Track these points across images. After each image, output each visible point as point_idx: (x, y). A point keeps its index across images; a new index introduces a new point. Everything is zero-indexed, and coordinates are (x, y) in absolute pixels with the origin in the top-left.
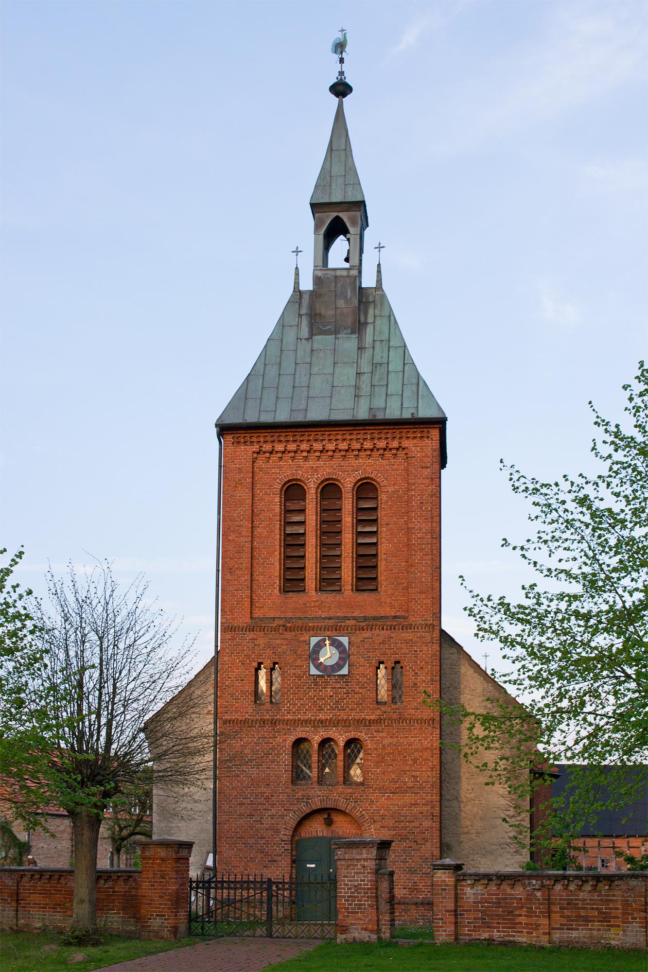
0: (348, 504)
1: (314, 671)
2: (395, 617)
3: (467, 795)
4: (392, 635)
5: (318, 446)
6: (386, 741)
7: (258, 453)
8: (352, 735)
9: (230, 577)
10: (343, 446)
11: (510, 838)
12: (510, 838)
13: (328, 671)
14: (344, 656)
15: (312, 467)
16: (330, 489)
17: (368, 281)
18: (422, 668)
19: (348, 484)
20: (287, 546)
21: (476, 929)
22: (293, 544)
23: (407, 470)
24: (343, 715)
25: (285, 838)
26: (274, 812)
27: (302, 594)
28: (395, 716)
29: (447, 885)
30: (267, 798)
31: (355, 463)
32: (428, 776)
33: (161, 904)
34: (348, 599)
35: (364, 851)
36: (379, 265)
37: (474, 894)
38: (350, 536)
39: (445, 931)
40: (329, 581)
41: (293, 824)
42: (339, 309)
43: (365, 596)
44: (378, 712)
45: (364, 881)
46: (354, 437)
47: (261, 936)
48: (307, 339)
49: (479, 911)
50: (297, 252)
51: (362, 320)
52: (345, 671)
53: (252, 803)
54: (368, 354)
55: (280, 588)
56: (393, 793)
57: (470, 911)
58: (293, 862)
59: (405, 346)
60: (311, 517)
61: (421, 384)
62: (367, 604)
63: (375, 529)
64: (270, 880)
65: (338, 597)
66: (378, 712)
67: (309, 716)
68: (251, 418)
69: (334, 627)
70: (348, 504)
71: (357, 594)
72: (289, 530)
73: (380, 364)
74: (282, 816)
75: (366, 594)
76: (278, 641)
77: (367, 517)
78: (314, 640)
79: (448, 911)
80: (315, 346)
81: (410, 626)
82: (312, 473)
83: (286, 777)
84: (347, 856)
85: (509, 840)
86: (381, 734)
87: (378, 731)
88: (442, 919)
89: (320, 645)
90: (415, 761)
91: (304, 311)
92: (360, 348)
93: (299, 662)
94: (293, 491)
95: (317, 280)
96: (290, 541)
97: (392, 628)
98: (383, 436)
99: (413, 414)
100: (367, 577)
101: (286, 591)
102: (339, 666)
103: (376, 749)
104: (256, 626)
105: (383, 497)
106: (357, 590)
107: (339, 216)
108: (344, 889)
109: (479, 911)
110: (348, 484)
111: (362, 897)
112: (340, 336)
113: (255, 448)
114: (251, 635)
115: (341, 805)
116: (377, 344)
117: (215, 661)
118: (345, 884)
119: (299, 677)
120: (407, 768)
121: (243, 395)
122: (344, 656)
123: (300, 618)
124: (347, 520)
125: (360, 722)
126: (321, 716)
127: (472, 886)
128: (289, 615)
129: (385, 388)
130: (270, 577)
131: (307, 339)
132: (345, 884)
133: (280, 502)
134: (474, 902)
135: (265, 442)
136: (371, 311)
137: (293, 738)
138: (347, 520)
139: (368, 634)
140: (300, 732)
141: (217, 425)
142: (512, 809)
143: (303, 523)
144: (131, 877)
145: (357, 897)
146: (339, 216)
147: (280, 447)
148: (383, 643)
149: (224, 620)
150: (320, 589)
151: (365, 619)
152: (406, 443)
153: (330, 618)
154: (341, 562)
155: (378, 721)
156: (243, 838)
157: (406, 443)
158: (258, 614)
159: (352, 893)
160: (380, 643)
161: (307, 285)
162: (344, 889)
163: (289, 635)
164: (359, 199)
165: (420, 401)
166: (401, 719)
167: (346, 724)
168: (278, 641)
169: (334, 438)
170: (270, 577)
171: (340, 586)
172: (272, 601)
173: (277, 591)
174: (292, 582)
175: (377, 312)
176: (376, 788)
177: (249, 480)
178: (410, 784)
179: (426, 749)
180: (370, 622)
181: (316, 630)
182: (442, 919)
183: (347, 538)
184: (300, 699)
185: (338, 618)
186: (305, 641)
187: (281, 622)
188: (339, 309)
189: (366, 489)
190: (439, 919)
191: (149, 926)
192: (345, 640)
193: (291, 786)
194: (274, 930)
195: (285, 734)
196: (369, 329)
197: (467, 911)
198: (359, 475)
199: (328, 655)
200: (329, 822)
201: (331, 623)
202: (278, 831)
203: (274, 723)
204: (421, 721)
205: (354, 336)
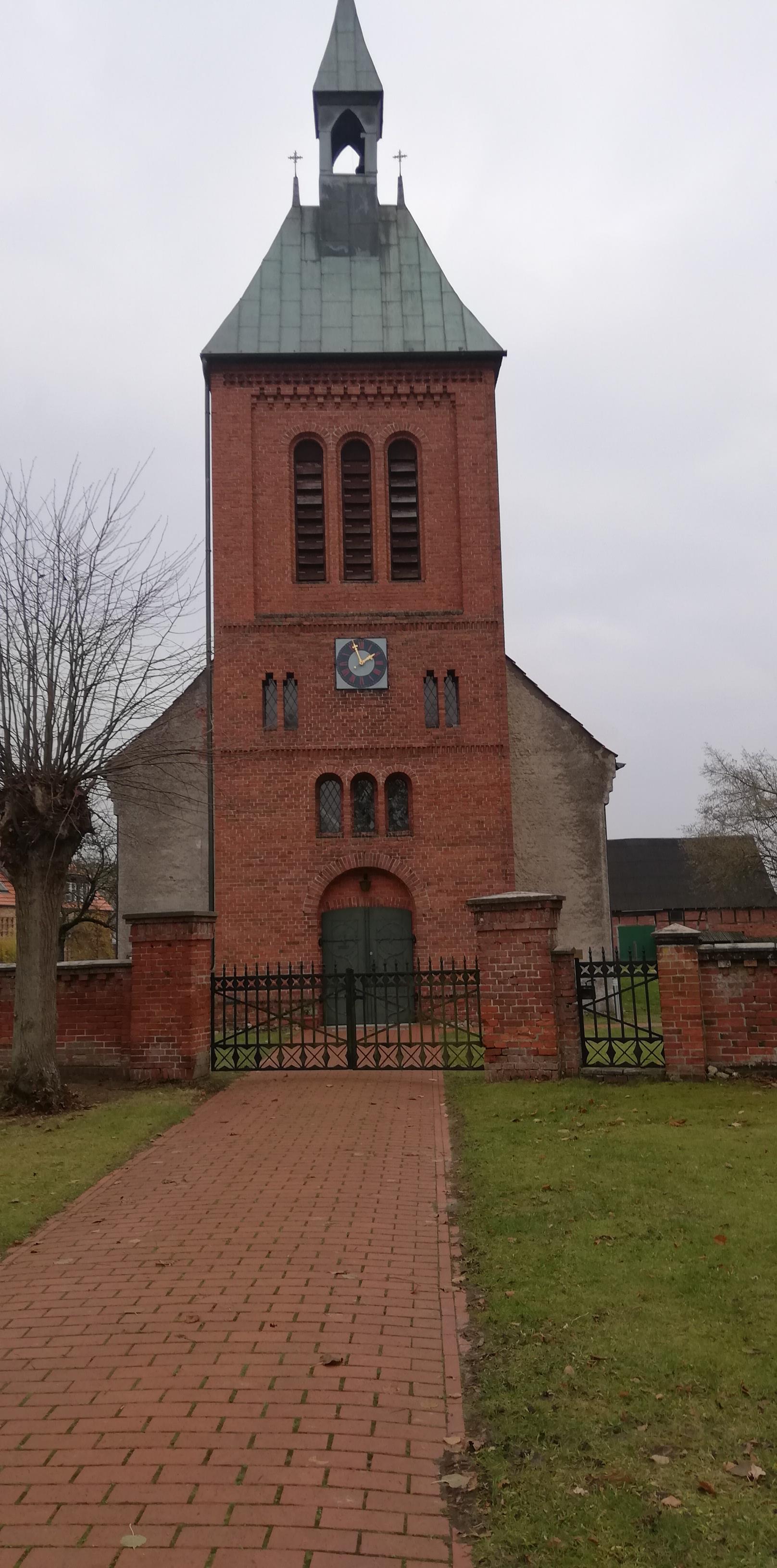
0: (379, 467)
1: (342, 684)
2: (445, 613)
3: (529, 850)
4: (443, 636)
5: (337, 389)
6: (441, 776)
7: (258, 397)
8: (396, 768)
9: (225, 560)
10: (371, 389)
11: (585, 904)
12: (585, 904)
13: (361, 689)
14: (380, 663)
15: (330, 418)
16: (355, 448)
17: (386, 196)
18: (483, 678)
19: (379, 439)
20: (299, 521)
21: (739, 1048)
22: (308, 519)
23: (454, 423)
24: (382, 743)
25: (309, 910)
26: (292, 874)
27: (322, 584)
28: (451, 742)
29: (683, 971)
30: (283, 856)
31: (386, 412)
32: (497, 822)
33: (167, 1020)
34: (383, 592)
35: (527, 916)
36: (400, 179)
37: (730, 986)
38: (383, 507)
39: (686, 1053)
40: (358, 567)
41: (318, 890)
42: (350, 225)
43: (404, 586)
44: (429, 738)
45: (529, 967)
46: (385, 378)
47: (338, 1067)
48: (314, 261)
49: (741, 1015)
50: (295, 158)
51: (383, 240)
52: (383, 683)
53: (262, 864)
54: (393, 281)
55: (292, 577)
56: (452, 845)
57: (726, 1015)
58: (321, 943)
59: (441, 272)
60: (333, 484)
61: (466, 315)
62: (407, 597)
63: (414, 500)
64: (350, 971)
65: (371, 587)
66: (429, 738)
67: (336, 744)
68: (249, 347)
69: (366, 628)
70: (379, 467)
71: (394, 583)
72: (302, 500)
73: (412, 292)
74: (304, 881)
75: (406, 583)
76: (293, 645)
77: (404, 484)
78: (340, 644)
79: (690, 1017)
80: (326, 269)
81: (466, 624)
82: (332, 425)
83: (308, 827)
84: (497, 926)
85: (583, 907)
86: (433, 767)
87: (429, 763)
88: (679, 1032)
89: (348, 651)
90: (479, 802)
91: (308, 228)
92: (384, 274)
93: (321, 674)
94: (307, 449)
95: (325, 188)
96: (303, 515)
97: (443, 626)
98: (423, 378)
99: (460, 348)
100: (407, 561)
101: (299, 580)
102: (375, 676)
103: (427, 786)
104: (264, 624)
105: (424, 457)
106: (394, 579)
107: (349, 112)
108: (493, 982)
109: (741, 1015)
110: (379, 439)
111: (526, 996)
112: (355, 258)
113: (255, 390)
114: (255, 637)
115: (384, 863)
116: (405, 269)
117: (207, 676)
118: (494, 975)
119: (322, 692)
120: (470, 811)
121: (236, 321)
122: (380, 663)
123: (322, 615)
124: (380, 486)
125: (406, 751)
126: (354, 744)
127: (725, 972)
128: (305, 611)
129: (421, 318)
130: (279, 561)
131: (314, 261)
132: (494, 975)
133: (289, 462)
134: (731, 1001)
135: (268, 383)
136: (393, 231)
137: (316, 774)
138: (380, 486)
139: (410, 635)
140: (326, 766)
141: (203, 356)
142: (585, 867)
143: (319, 492)
144: (112, 975)
145: (517, 996)
146: (349, 112)
147: (287, 390)
148: (432, 646)
149: (219, 617)
150: (346, 578)
151: (407, 615)
152: (452, 388)
153: (360, 615)
154: (371, 543)
155: (430, 749)
156: (251, 912)
157: (452, 388)
158: (266, 610)
159: (507, 989)
160: (428, 647)
161: (311, 198)
162: (493, 982)
163: (307, 637)
164: (376, 88)
165: (467, 334)
166: (459, 747)
167: (386, 753)
168: (293, 645)
169: (358, 379)
170: (279, 561)
171: (371, 574)
172: (283, 591)
173: (288, 580)
174: (309, 567)
175: (401, 233)
176: (429, 840)
177: (248, 432)
178: (476, 833)
179: (493, 785)
180: (411, 621)
181: (344, 629)
182: (679, 1032)
183: (380, 512)
184: (323, 721)
185: (372, 615)
186: (328, 645)
187: (295, 620)
188: (350, 225)
189: (403, 448)
190: (674, 1032)
191: (145, 1059)
192: (381, 643)
193: (315, 839)
194: (361, 1056)
195: (306, 769)
196: (393, 252)
197: (718, 1015)
198: (391, 428)
199: (361, 662)
200: (366, 887)
201: (363, 620)
202: (298, 901)
203: (290, 753)
204: (484, 748)
205: (375, 259)
